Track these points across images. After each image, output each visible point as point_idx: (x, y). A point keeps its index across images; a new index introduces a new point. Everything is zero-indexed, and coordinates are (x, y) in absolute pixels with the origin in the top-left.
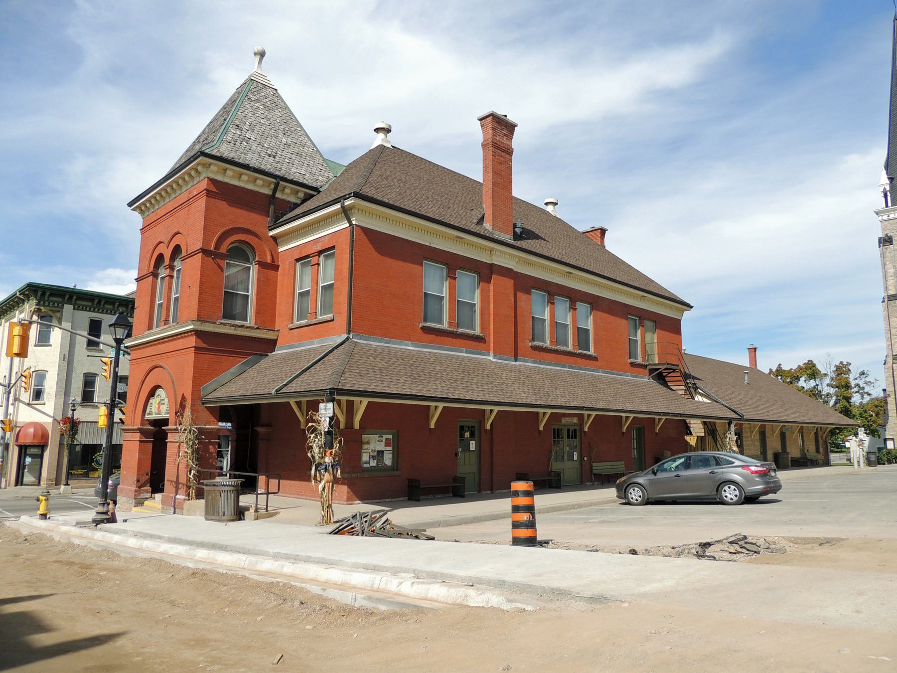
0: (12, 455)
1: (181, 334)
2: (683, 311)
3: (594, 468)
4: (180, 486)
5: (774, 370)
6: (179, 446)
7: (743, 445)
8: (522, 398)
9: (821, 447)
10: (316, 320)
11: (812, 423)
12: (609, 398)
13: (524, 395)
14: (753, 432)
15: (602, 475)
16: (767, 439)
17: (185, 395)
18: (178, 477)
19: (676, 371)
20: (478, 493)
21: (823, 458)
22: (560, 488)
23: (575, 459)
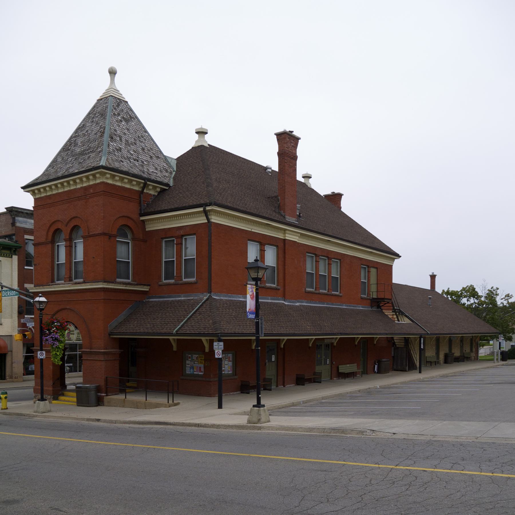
3: (340, 369)
5: (445, 291)
7: (425, 349)
8: (309, 330)
9: (474, 347)
10: (181, 282)
11: (470, 334)
12: (353, 325)
13: (309, 328)
14: (432, 340)
15: (345, 373)
16: (440, 344)
19: (390, 303)
20: (276, 387)
21: (474, 355)
22: (321, 383)
23: (328, 363)
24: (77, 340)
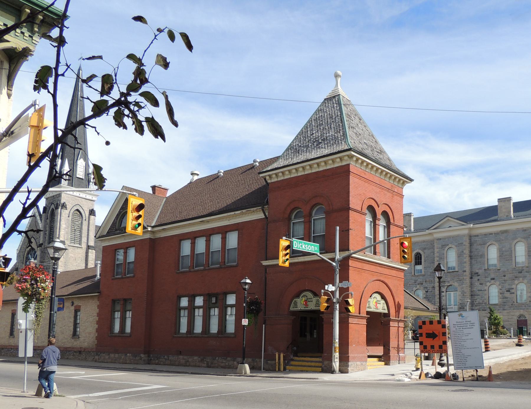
0: (316, 362)
1: (386, 266)
2: (404, 183)
4: (400, 349)
6: (398, 329)
17: (399, 302)
18: (398, 345)
24: (383, 310)
